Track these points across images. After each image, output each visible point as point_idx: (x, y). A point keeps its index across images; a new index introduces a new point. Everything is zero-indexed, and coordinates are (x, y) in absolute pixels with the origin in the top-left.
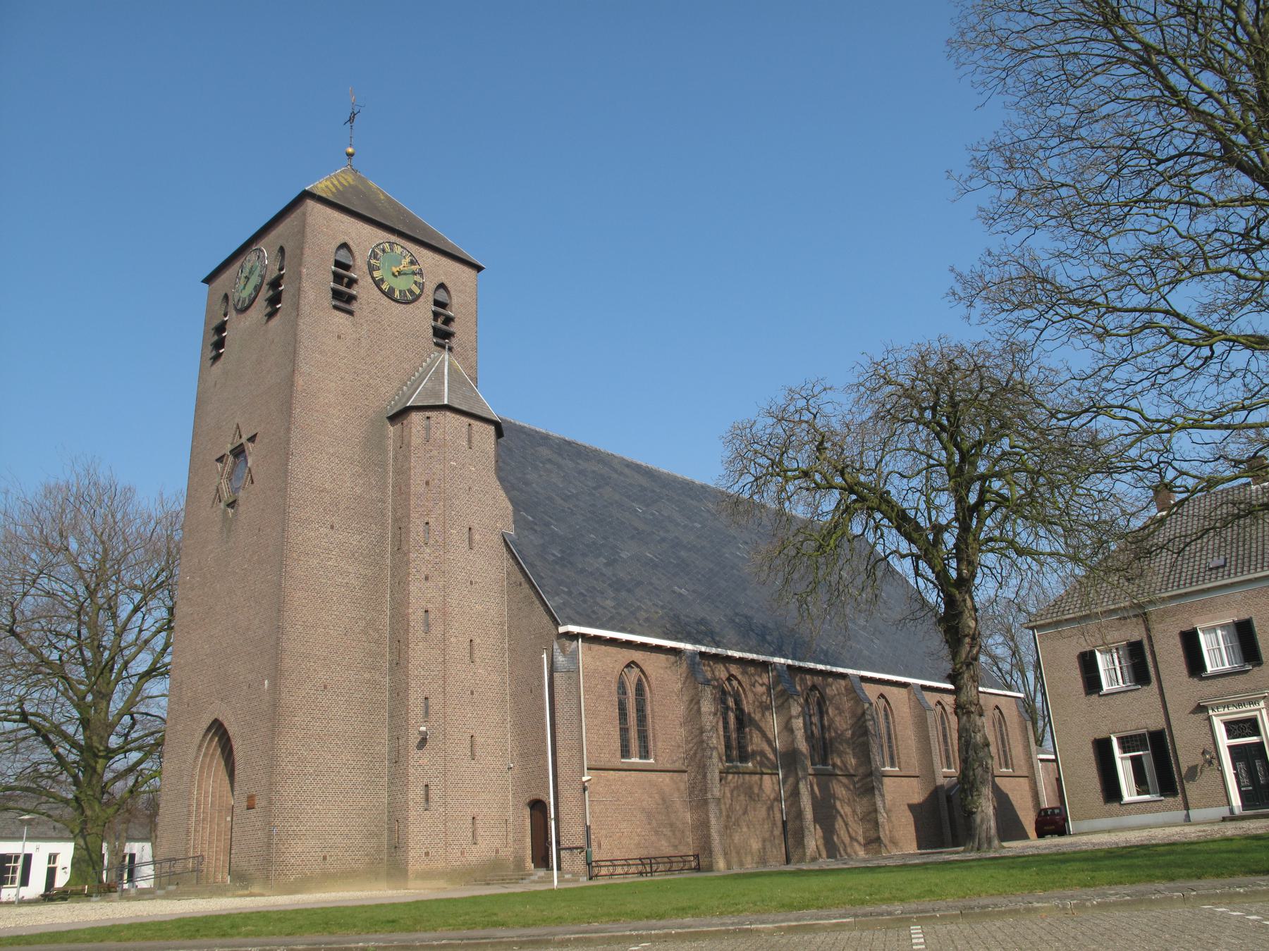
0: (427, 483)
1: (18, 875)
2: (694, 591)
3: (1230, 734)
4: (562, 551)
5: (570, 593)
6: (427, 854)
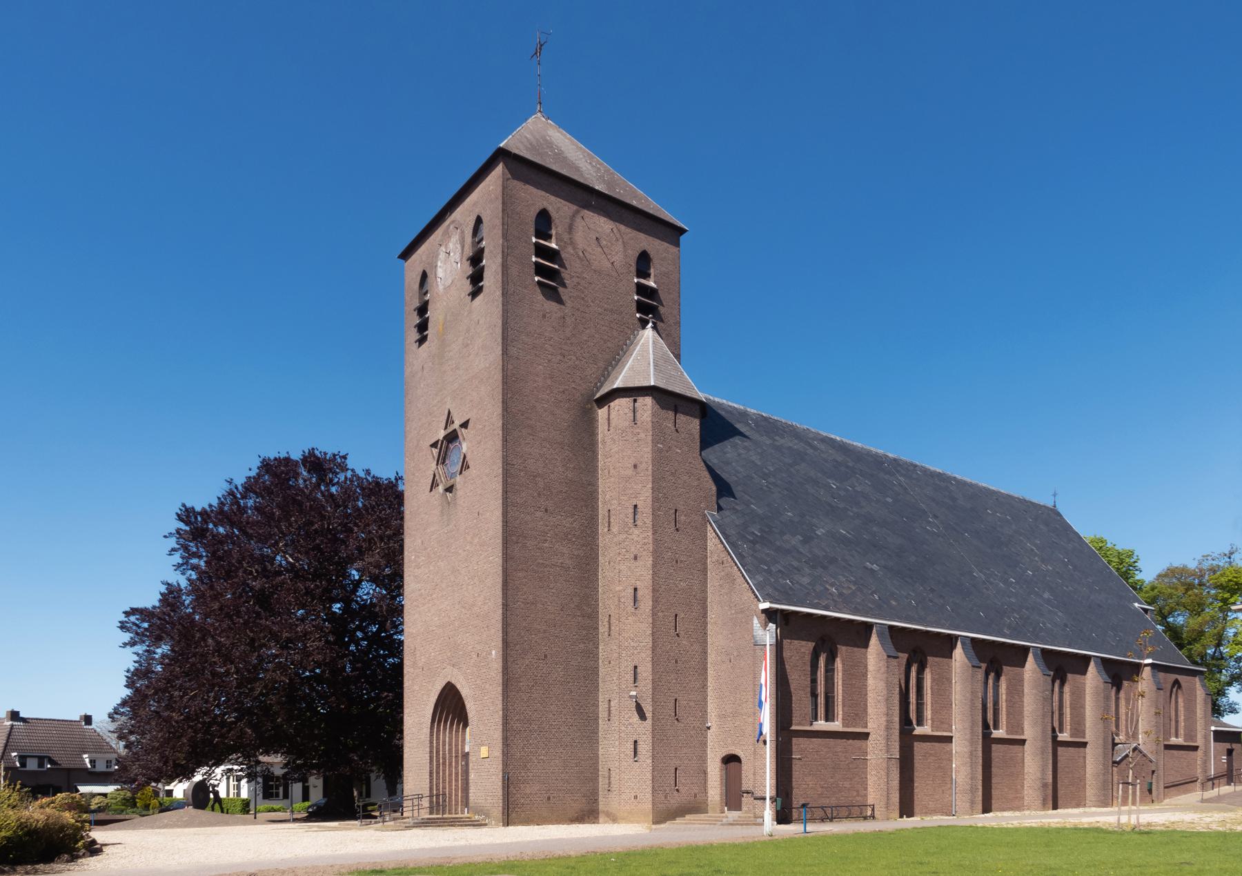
0: (635, 466)
1: (879, 752)
2: (885, 567)
3: (695, 807)
4: (761, 530)
5: (769, 572)
6: (636, 797)
